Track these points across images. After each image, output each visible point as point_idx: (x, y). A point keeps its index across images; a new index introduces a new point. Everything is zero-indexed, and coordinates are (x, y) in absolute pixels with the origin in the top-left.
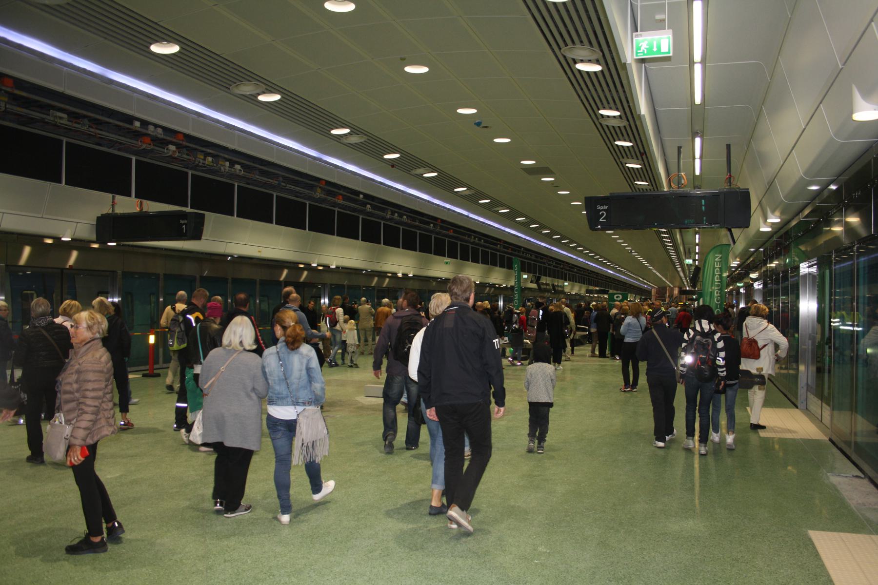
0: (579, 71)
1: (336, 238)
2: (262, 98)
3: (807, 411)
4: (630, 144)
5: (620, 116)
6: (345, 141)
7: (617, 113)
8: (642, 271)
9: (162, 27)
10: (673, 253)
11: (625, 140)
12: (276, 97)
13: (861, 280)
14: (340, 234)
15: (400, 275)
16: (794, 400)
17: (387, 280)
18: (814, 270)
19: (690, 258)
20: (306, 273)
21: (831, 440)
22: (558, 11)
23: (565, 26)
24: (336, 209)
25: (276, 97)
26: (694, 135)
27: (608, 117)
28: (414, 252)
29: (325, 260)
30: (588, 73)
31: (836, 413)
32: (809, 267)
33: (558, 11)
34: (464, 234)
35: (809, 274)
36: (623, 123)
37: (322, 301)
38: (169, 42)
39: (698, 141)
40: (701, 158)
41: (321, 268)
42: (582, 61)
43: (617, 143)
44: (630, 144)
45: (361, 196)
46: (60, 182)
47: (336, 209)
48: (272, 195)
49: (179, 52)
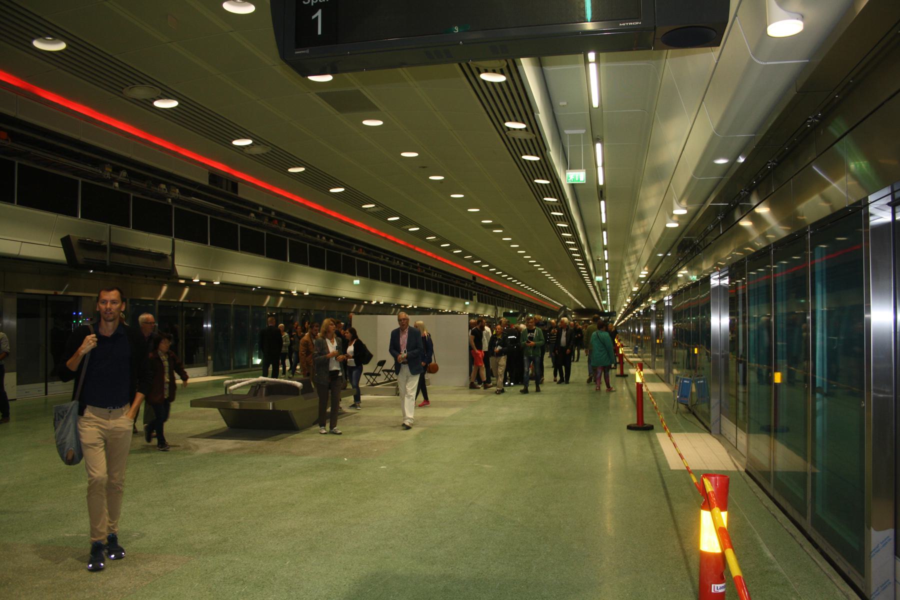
0: (484, 81)
1: (308, 268)
2: (159, 104)
3: (720, 435)
4: (547, 182)
5: (526, 129)
6: (247, 151)
7: (523, 126)
8: (558, 295)
9: (45, 20)
10: (596, 298)
11: (543, 179)
12: (174, 104)
13: (819, 287)
14: (21, 203)
15: (294, 293)
16: (707, 424)
17: (282, 299)
18: (726, 281)
19: (599, 275)
20: (186, 290)
21: (746, 471)
22: (495, 89)
23: (503, 105)
24: (342, 254)
25: (174, 104)
26: (596, 140)
27: (514, 129)
28: (322, 271)
29: (301, 288)
30: (492, 83)
31: (752, 436)
32: (720, 278)
33: (495, 89)
34: (144, 179)
35: (720, 286)
36: (529, 136)
37: (671, 327)
38: (54, 38)
39: (605, 233)
40: (603, 166)
41: (203, 284)
42: (486, 71)
43: (525, 157)
44: (547, 182)
45: (273, 213)
46: (286, 260)
47: (80, 180)
48: (14, 163)
49: (66, 49)
